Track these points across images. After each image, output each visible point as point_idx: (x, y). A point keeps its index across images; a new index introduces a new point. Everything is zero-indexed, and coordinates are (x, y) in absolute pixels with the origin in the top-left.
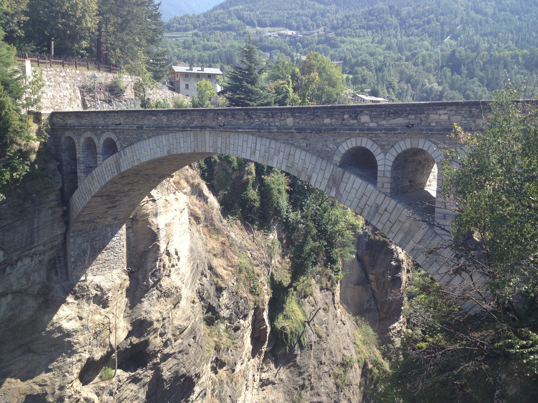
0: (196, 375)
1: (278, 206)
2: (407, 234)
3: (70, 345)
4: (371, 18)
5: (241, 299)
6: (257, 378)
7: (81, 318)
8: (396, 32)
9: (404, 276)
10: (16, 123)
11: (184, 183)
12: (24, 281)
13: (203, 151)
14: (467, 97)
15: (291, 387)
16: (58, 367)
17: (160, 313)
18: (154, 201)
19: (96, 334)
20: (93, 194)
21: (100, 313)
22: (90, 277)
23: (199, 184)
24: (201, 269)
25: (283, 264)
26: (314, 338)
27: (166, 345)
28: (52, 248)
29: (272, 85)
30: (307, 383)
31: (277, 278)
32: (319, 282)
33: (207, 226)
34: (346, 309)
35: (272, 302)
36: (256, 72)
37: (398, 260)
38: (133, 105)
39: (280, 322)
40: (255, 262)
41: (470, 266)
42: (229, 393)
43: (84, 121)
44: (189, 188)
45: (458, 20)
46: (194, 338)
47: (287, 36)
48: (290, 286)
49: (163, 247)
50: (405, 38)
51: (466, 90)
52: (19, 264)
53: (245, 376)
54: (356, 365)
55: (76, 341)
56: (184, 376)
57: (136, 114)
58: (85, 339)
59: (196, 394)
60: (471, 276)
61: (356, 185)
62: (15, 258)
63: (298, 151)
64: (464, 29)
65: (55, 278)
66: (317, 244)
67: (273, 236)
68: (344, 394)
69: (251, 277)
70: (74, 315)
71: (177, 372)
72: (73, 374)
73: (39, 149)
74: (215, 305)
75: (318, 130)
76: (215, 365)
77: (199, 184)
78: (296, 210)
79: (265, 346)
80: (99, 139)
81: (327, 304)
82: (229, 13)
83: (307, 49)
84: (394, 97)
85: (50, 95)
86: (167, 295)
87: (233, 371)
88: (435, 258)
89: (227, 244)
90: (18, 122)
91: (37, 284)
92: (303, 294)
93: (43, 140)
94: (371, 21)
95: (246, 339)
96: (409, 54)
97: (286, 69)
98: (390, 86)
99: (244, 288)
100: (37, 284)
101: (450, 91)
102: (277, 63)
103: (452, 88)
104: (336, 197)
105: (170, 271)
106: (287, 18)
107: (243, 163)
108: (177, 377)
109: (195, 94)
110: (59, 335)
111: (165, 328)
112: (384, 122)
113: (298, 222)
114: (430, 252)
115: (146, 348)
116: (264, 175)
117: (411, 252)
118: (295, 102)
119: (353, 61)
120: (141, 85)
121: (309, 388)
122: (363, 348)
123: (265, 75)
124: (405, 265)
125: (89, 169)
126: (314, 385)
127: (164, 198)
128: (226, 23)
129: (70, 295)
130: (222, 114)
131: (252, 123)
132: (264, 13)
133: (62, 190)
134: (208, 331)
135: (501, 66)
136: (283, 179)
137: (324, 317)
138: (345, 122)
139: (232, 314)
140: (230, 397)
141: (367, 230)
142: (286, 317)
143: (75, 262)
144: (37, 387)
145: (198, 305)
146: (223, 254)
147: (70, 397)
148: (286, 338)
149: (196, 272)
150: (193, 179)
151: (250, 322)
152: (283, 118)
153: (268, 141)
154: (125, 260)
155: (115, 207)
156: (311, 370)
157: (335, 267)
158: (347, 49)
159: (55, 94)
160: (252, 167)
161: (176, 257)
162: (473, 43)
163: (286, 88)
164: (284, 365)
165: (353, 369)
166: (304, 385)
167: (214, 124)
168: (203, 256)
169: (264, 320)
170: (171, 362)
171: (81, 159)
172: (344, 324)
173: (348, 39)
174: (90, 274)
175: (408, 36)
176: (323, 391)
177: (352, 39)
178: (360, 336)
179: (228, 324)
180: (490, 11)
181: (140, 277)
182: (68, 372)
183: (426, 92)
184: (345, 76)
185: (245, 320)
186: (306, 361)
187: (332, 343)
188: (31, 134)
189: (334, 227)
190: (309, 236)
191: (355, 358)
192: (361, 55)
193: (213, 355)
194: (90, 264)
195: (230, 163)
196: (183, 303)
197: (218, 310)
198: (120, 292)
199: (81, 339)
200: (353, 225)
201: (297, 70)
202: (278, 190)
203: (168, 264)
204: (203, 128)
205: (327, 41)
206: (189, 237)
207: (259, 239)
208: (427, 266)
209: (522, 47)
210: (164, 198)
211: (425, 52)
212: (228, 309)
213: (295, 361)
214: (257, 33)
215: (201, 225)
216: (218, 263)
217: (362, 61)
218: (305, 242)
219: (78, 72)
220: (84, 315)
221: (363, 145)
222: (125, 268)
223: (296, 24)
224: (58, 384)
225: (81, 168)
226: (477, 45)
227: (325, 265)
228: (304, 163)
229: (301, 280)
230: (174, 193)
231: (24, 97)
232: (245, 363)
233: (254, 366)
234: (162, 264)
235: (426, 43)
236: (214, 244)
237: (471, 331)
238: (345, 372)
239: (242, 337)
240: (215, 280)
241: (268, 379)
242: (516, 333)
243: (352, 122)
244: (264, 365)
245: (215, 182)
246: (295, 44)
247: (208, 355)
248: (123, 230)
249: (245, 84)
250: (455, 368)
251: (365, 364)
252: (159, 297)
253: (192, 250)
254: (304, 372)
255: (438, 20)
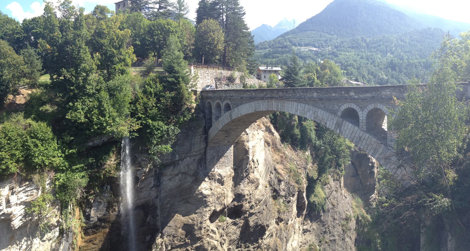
0: (267, 225)
1: (310, 138)
2: (375, 150)
3: (206, 202)
4: (354, 43)
5: (291, 186)
6: (301, 228)
7: (211, 189)
8: (365, 50)
9: (376, 171)
10: (187, 95)
11: (262, 126)
12: (186, 168)
13: (272, 110)
14: (399, 82)
15: (319, 232)
16: (200, 212)
17: (249, 191)
18: (247, 134)
19: (218, 198)
20: (219, 129)
21: (220, 188)
22: (216, 170)
23: (269, 126)
24: (270, 170)
25: (314, 168)
26: (330, 206)
27: (251, 208)
28: (200, 154)
29: (306, 76)
30: (327, 230)
31: (310, 175)
32: (333, 176)
33: (273, 148)
34: (347, 190)
35: (308, 188)
36: (297, 69)
37: (373, 163)
38: (239, 87)
39: (313, 199)
40: (298, 167)
41: (404, 164)
42: (285, 236)
43: (216, 95)
44: (265, 128)
45: (393, 45)
46: (266, 206)
47: (313, 51)
48: (317, 179)
49: (251, 158)
50: (369, 53)
51: (399, 78)
52: (185, 160)
53: (293, 227)
54: (353, 219)
55: (208, 200)
56: (260, 225)
57: (240, 91)
58: (213, 200)
59: (266, 235)
60: (405, 169)
61: (349, 127)
62: (183, 157)
63: (320, 110)
64: (396, 49)
65: (200, 168)
66: (331, 157)
67: (308, 153)
68: (347, 235)
69: (296, 176)
70: (208, 187)
71: (257, 223)
72: (206, 217)
73: (196, 107)
74: (277, 189)
75: (329, 99)
76: (277, 221)
77: (269, 126)
78: (320, 140)
79: (305, 211)
80: (222, 103)
81: (337, 188)
82: (285, 39)
83: (323, 57)
84: (366, 82)
85: (201, 82)
86: (252, 182)
87: (287, 224)
88: (388, 161)
89: (284, 157)
90: (187, 95)
91: (192, 170)
92: (324, 183)
93: (197, 103)
94: (354, 44)
95: (294, 207)
96: (371, 61)
97: (313, 68)
98: (363, 77)
99: (292, 181)
100: (192, 170)
101: (391, 79)
102: (308, 64)
103: (392, 77)
104: (339, 133)
105: (254, 170)
106: (313, 42)
107: (291, 116)
108: (257, 225)
109: (268, 81)
110: (201, 196)
111: (251, 199)
112: (361, 96)
113: (321, 146)
114: (386, 159)
115: (241, 208)
116: (303, 122)
117: (377, 159)
118: (318, 84)
119: (346, 64)
120: (243, 77)
121: (328, 233)
122: (357, 210)
123: (302, 71)
124: (376, 165)
125: (218, 118)
126: (331, 231)
127: (252, 133)
128: (284, 44)
129: (207, 177)
130: (281, 91)
131: (296, 96)
132: (301, 40)
133: (205, 127)
134: (274, 202)
135: (414, 67)
136: (312, 124)
137: (336, 195)
138: (343, 95)
139: (286, 194)
140: (286, 237)
141: (356, 149)
142: (316, 196)
143: (209, 162)
144: (190, 221)
145: (269, 188)
146: (282, 163)
147: (205, 228)
148: (316, 207)
149: (267, 171)
150: (267, 123)
151: (296, 198)
152: (311, 93)
153: (304, 105)
154: (232, 163)
155: (229, 136)
156: (329, 223)
157: (341, 168)
158: (343, 58)
159: (204, 82)
160: (296, 118)
161: (257, 163)
162: (401, 56)
163: (313, 77)
164: (315, 221)
165: (352, 221)
166: (326, 231)
167: (277, 96)
168: (271, 163)
169: (304, 197)
170: (254, 217)
171: (214, 113)
172: (346, 198)
173: (343, 53)
174: (216, 168)
175: (371, 52)
176: (336, 234)
177: (345, 53)
178: (355, 204)
179: (284, 199)
180: (407, 41)
181: (239, 172)
182: (204, 215)
183: (381, 80)
184: (342, 71)
185: (293, 197)
186: (327, 219)
187: (340, 208)
188: (193, 100)
189: (340, 147)
190: (327, 153)
191: (352, 215)
192: (350, 61)
193: (276, 215)
194: (216, 163)
195: (285, 115)
196: (260, 187)
197: (279, 191)
198: (230, 178)
199: (211, 199)
200: (349, 147)
201: (319, 68)
202: (310, 129)
203: (253, 166)
204: (272, 98)
205: (333, 53)
206: (264, 153)
207: (300, 155)
208: (385, 165)
209: (422, 58)
210: (252, 133)
211: (379, 60)
212: (285, 191)
213: (321, 219)
214: (298, 50)
215: (270, 147)
216: (279, 167)
217: (350, 64)
218: (325, 156)
219: (214, 71)
220: (213, 188)
221: (352, 107)
222: (232, 167)
223: (317, 45)
224: (199, 221)
225: (214, 117)
226: (403, 57)
227: (336, 168)
228: (323, 116)
229: (323, 176)
230: (257, 130)
231: (190, 83)
232: (293, 220)
233: (299, 222)
234: (250, 166)
235: (379, 56)
236: (277, 157)
237: (407, 196)
238: (347, 223)
239: (292, 206)
240: (278, 176)
241: (307, 229)
242: (427, 195)
243: (346, 95)
244: (305, 221)
245: (278, 125)
246: (317, 55)
247: (274, 215)
248: (232, 148)
249: (293, 75)
250: (401, 216)
251: (358, 218)
252: (248, 183)
253: (265, 160)
254: (326, 224)
255: (384, 45)
